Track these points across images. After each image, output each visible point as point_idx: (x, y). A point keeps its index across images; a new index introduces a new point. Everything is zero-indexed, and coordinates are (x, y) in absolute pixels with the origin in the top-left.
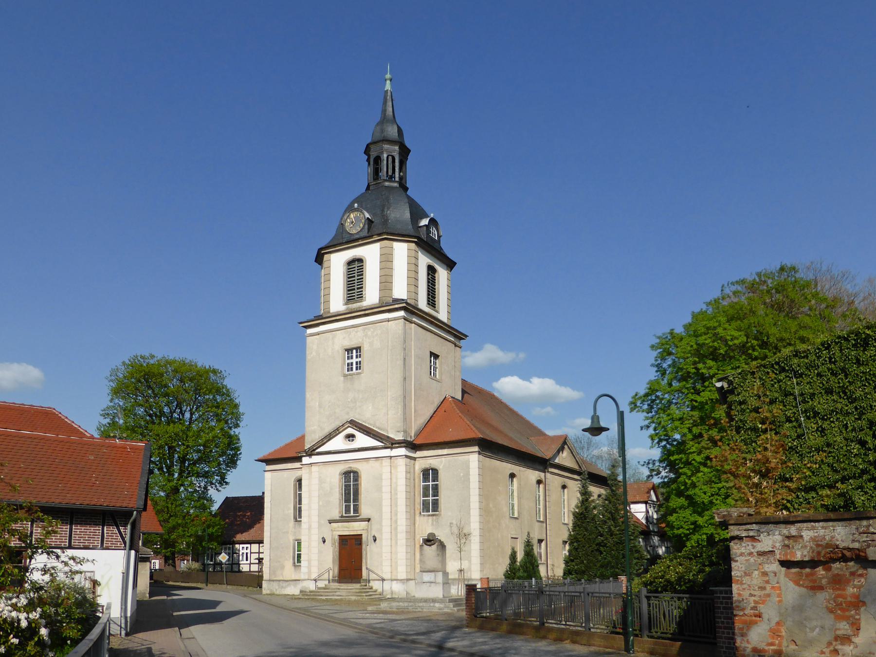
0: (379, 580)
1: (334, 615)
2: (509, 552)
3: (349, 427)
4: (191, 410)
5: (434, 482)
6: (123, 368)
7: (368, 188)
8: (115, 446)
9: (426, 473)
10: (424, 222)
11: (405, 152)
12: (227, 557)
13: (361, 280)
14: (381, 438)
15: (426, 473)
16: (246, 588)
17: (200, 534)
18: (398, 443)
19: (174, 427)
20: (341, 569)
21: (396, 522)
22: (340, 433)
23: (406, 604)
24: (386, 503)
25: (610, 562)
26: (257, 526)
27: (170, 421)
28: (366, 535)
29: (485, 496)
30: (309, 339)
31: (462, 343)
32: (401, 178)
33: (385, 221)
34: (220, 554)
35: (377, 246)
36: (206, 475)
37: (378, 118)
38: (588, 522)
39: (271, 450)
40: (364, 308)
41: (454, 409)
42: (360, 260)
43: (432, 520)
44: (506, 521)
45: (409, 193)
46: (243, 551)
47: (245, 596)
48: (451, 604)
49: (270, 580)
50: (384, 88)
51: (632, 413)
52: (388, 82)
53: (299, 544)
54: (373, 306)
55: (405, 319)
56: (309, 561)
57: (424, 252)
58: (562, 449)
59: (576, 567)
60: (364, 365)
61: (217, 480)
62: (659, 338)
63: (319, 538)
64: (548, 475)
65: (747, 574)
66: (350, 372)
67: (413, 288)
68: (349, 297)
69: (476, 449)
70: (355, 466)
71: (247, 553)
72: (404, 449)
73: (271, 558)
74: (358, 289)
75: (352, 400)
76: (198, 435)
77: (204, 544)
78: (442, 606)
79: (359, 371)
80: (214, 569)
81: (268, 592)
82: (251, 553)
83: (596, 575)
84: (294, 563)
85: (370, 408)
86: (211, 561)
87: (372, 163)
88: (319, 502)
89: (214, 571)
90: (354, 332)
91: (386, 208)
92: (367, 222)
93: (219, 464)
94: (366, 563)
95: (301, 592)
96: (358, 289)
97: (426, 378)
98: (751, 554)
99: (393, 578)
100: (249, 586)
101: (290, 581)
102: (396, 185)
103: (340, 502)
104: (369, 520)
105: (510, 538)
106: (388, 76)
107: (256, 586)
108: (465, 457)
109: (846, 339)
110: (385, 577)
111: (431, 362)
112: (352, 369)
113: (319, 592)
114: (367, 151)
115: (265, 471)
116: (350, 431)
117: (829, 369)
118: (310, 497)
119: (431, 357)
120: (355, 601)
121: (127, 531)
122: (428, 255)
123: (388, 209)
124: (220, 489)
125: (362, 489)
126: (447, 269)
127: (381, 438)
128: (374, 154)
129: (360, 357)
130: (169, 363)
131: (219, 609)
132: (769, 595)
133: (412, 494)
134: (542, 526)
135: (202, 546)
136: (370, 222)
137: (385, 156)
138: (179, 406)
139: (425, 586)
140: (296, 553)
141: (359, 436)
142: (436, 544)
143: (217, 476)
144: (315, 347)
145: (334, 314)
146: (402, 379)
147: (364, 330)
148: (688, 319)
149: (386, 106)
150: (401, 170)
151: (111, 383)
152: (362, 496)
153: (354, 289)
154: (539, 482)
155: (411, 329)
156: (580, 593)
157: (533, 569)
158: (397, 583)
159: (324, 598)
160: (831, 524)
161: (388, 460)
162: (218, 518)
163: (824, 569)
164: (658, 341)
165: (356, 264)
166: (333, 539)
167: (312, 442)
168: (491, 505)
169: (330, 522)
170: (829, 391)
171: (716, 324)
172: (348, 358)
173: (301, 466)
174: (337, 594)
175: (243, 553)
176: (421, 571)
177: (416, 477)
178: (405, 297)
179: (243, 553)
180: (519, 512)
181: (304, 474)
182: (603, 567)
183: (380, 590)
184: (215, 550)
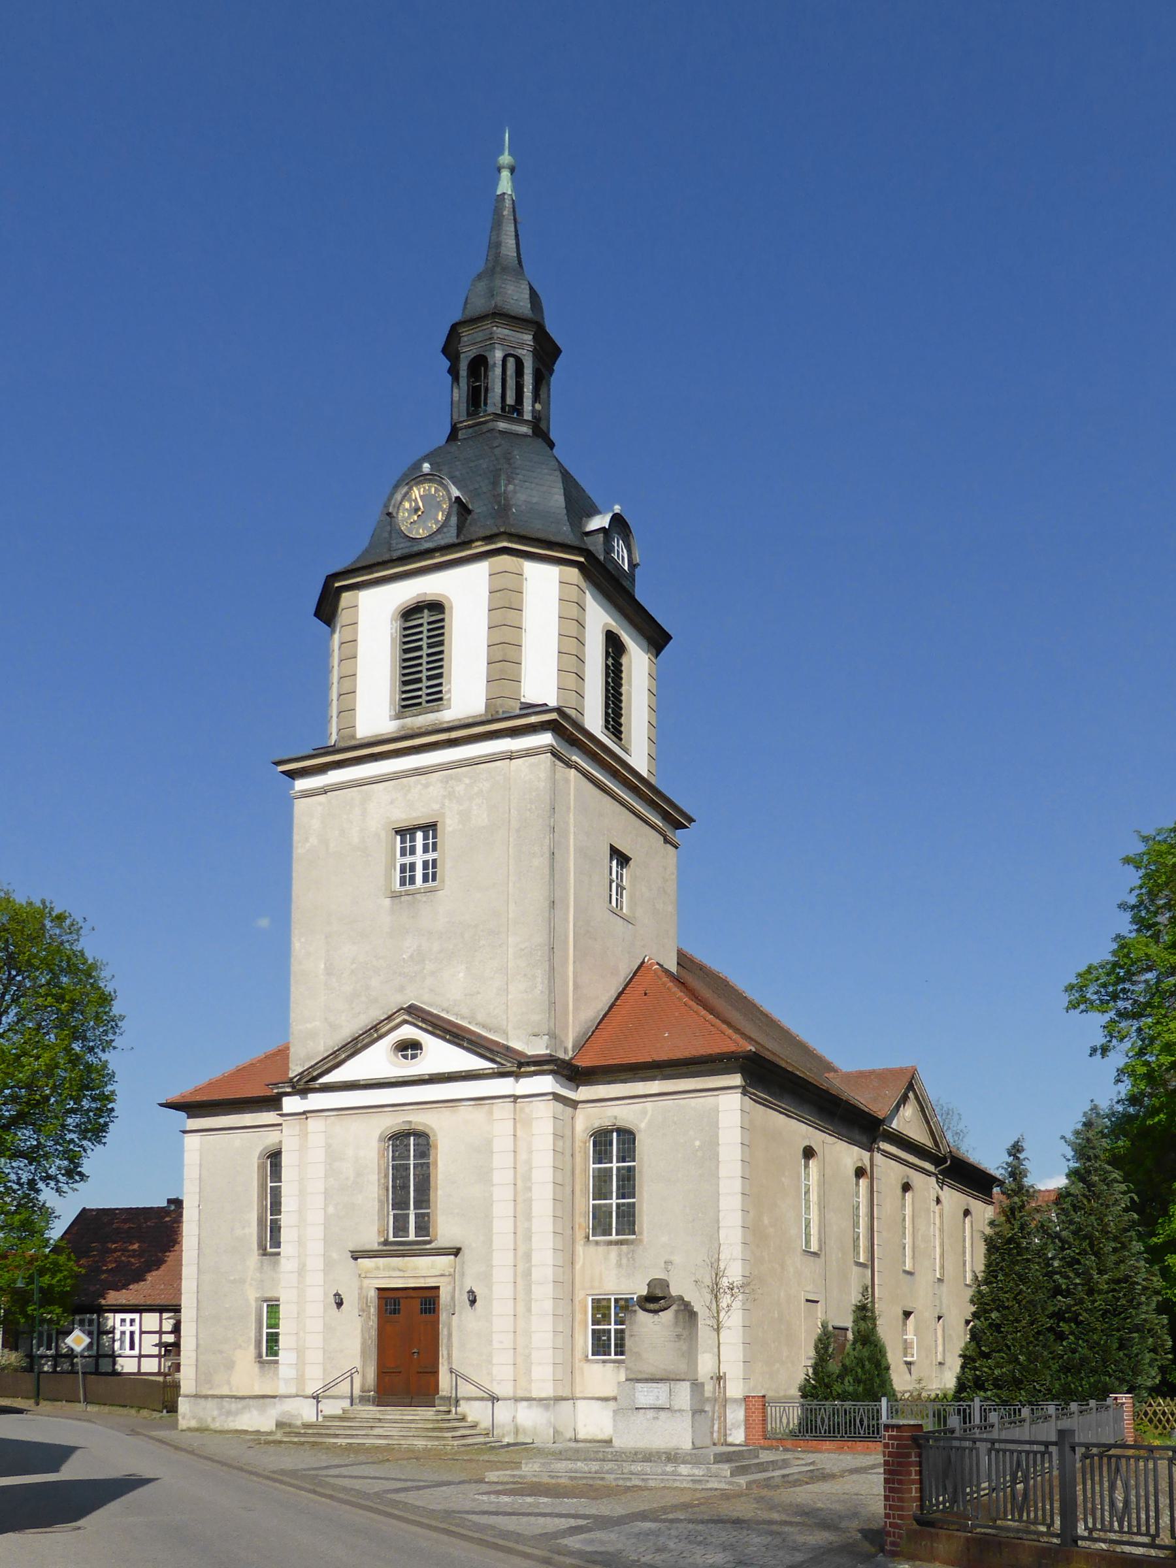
0: (482, 1399)
1: (411, 1498)
5: (624, 1161)
9: (601, 1139)
10: (600, 522)
12: (87, 1340)
13: (437, 658)
14: (491, 1051)
15: (601, 1139)
16: (133, 1412)
17: (19, 1285)
18: (535, 1063)
20: (382, 1372)
21: (528, 1256)
22: (380, 1037)
23: (595, 1466)
24: (502, 1211)
25: (1084, 1360)
28: (450, 1288)
30: (300, 805)
31: (679, 836)
33: (503, 509)
34: (69, 1333)
35: (479, 571)
36: (32, 1156)
38: (1028, 1260)
40: (445, 725)
41: (664, 984)
42: (436, 607)
43: (620, 1255)
44: (796, 1262)
46: (123, 1329)
47: (134, 1432)
48: (726, 1466)
49: (196, 1396)
50: (496, 190)
51: (1072, 1012)
52: (505, 174)
53: (273, 1308)
55: (554, 754)
56: (300, 1352)
57: (600, 597)
59: (997, 1372)
60: (447, 870)
61: (59, 1168)
62: (1145, 839)
63: (325, 1294)
64: (878, 1157)
66: (408, 887)
68: (404, 699)
69: (737, 1080)
71: (132, 1333)
72: (549, 1079)
73: (201, 1342)
74: (429, 678)
75: (411, 957)
78: (698, 1472)
79: (430, 884)
80: (55, 1366)
81: (193, 1424)
82: (142, 1332)
83: (1049, 1390)
84: (260, 1356)
85: (461, 975)
86: (49, 1348)
87: (463, 372)
88: (326, 1206)
89: (55, 1372)
90: (420, 787)
91: (503, 477)
92: (455, 509)
94: (449, 1356)
95: (280, 1425)
97: (600, 912)
100: (141, 1408)
101: (250, 1397)
102: (524, 429)
103: (381, 1210)
104: (456, 1252)
105: (803, 1300)
106: (506, 159)
107: (160, 1408)
108: (708, 1101)
110: (498, 1391)
112: (412, 880)
113: (328, 1427)
114: (450, 350)
115: (185, 1132)
116: (408, 1032)
118: (302, 1193)
119: (611, 862)
120: (426, 1450)
122: (605, 602)
123: (510, 481)
124: (65, 1188)
125: (440, 1176)
126: (648, 651)
127: (491, 1051)
128: (467, 353)
129: (435, 849)
131: (69, 1472)
133: (568, 1189)
135: (26, 1316)
136: (462, 509)
137: (499, 355)
140: (265, 1331)
141: (429, 1041)
142: (674, 1308)
144: (316, 824)
146: (546, 904)
147: (446, 781)
150: (536, 398)
152: (440, 1192)
154: (860, 1172)
155: (567, 781)
156: (1047, 1444)
158: (529, 1407)
161: (508, 1106)
164: (1141, 848)
165: (426, 616)
166: (363, 1298)
167: (309, 1058)
168: (766, 1221)
169: (356, 1256)
173: (279, 1120)
174: (376, 1432)
175: (123, 1333)
176: (627, 1380)
177: (577, 1149)
178: (553, 703)
180: (820, 1240)
181: (289, 1138)
182: (1069, 1370)
183: (485, 1423)
184: (58, 1324)
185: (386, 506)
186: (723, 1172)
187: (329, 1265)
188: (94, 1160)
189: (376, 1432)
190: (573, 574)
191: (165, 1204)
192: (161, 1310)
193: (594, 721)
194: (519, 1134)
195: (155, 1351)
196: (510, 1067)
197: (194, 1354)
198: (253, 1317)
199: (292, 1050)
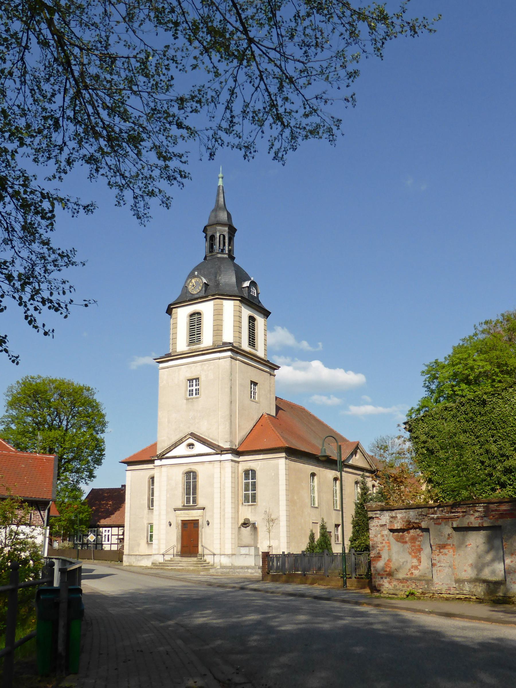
0: (211, 555)
2: (309, 533)
3: (190, 438)
4: (67, 419)
6: (17, 386)
7: (205, 258)
8: (36, 458)
9: (247, 473)
10: (247, 284)
11: (232, 231)
13: (199, 328)
15: (247, 473)
16: (109, 562)
19: (55, 433)
20: (183, 547)
21: (224, 510)
22: (183, 442)
24: (217, 496)
26: (117, 513)
27: (51, 428)
29: (291, 490)
30: (161, 372)
32: (230, 251)
33: (218, 285)
35: (211, 303)
36: (78, 471)
37: (213, 206)
39: (132, 454)
40: (202, 349)
42: (199, 314)
44: (308, 510)
45: (235, 261)
46: (105, 534)
47: (110, 567)
49: (129, 555)
52: (221, 179)
53: (152, 527)
54: (208, 348)
55: (231, 358)
56: (159, 540)
58: (354, 453)
60: (201, 391)
62: (427, 366)
65: (376, 536)
66: (191, 397)
67: (237, 334)
69: (284, 455)
70: (194, 468)
71: (108, 535)
72: (230, 455)
74: (197, 334)
76: (73, 440)
77: (75, 526)
78: (253, 571)
79: (197, 396)
81: (128, 564)
82: (112, 535)
84: (148, 542)
87: (208, 238)
93: (88, 462)
95: (152, 563)
96: (197, 334)
98: (377, 526)
99: (222, 553)
103: (182, 495)
104: (204, 509)
106: (220, 175)
109: (473, 400)
110: (215, 553)
111: (251, 389)
112: (192, 395)
114: (205, 230)
116: (191, 441)
117: (464, 418)
120: (193, 570)
121: (45, 514)
123: (220, 275)
124: (88, 482)
128: (210, 233)
130: (52, 381)
132: (384, 546)
133: (236, 489)
134: (339, 514)
135: (74, 529)
137: (218, 235)
138: (58, 415)
139: (242, 558)
140: (149, 533)
141: (196, 444)
143: (86, 472)
145: (179, 353)
148: (450, 352)
149: (219, 198)
150: (229, 244)
151: (8, 398)
153: (194, 335)
154: (336, 479)
155: (236, 364)
157: (327, 546)
159: (170, 568)
160: (408, 510)
162: (87, 506)
163: (408, 533)
164: (426, 368)
165: (196, 316)
166: (177, 523)
167: (163, 449)
168: (295, 498)
170: (465, 432)
171: (466, 356)
172: (190, 386)
174: (179, 565)
175: (105, 535)
178: (232, 341)
179: (105, 535)
180: (318, 503)
181: (156, 473)
183: (212, 563)
185: (185, 284)
186: (280, 483)
187: (167, 513)
188: (98, 471)
189: (179, 565)
190: (238, 302)
191: (120, 487)
192: (118, 526)
193: (245, 346)
194: (222, 472)
195: (116, 542)
196: (219, 452)
197: (128, 541)
198: (146, 530)
199: (158, 446)
